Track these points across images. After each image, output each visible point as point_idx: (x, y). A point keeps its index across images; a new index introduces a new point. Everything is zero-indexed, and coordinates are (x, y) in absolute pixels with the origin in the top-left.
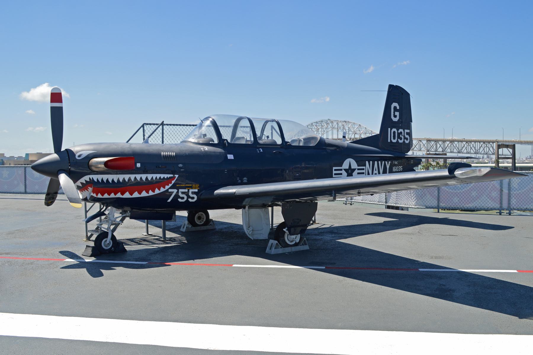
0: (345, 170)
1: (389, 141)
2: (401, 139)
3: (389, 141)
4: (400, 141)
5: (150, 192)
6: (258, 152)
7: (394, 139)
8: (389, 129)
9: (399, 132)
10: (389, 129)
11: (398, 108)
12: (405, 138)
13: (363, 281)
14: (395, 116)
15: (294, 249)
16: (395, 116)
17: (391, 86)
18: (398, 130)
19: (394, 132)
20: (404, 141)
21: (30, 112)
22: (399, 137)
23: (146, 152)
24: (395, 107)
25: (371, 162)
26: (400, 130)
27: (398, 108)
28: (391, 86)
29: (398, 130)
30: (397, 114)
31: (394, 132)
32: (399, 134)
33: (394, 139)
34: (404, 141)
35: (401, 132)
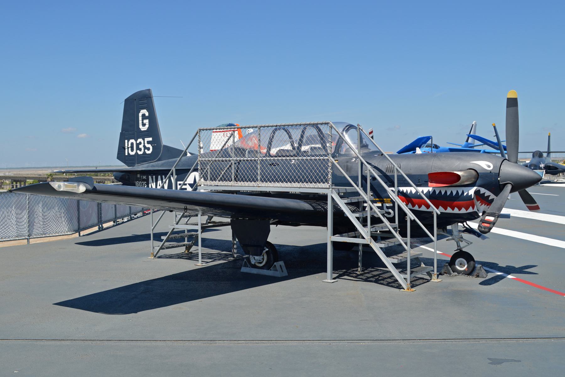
0: (190, 184)
1: (126, 154)
2: (140, 150)
3: (126, 154)
4: (140, 153)
6: (154, 187)
7: (132, 150)
8: (126, 141)
9: (138, 142)
10: (126, 141)
11: (147, 114)
12: (145, 147)
14: (144, 125)
15: (254, 271)
16: (144, 125)
17: (508, 99)
18: (136, 141)
19: (132, 144)
20: (137, 152)
21: (83, 135)
22: (138, 149)
23: (247, 205)
24: (143, 115)
25: (154, 177)
26: (140, 140)
27: (147, 114)
28: (508, 99)
29: (136, 141)
30: (146, 121)
31: (132, 144)
32: (138, 145)
33: (132, 150)
34: (137, 152)
35: (140, 143)
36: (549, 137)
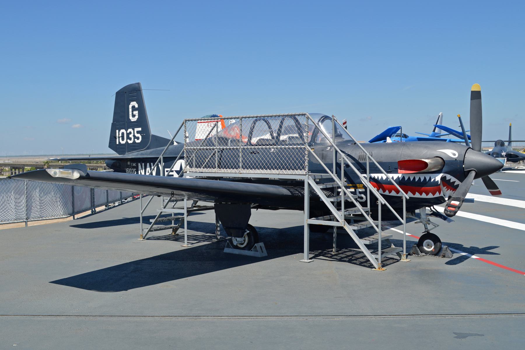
0: (176, 171)
1: (118, 143)
2: (130, 139)
3: (118, 143)
4: (130, 142)
5: (424, 194)
6: (143, 173)
7: (123, 139)
8: (117, 131)
9: (128, 132)
10: (117, 131)
11: (137, 106)
12: (135, 137)
13: (126, 290)
14: (134, 116)
15: (236, 252)
16: (134, 116)
17: (472, 92)
18: (127, 131)
19: (123, 134)
20: (127, 141)
22: (128, 138)
23: (229, 190)
24: (133, 107)
25: (143, 164)
26: (130, 130)
27: (137, 106)
28: (472, 92)
29: (127, 131)
30: (136, 113)
31: (123, 134)
32: (128, 134)
33: (123, 139)
34: (127, 141)
35: (130, 133)
36: (510, 127)
